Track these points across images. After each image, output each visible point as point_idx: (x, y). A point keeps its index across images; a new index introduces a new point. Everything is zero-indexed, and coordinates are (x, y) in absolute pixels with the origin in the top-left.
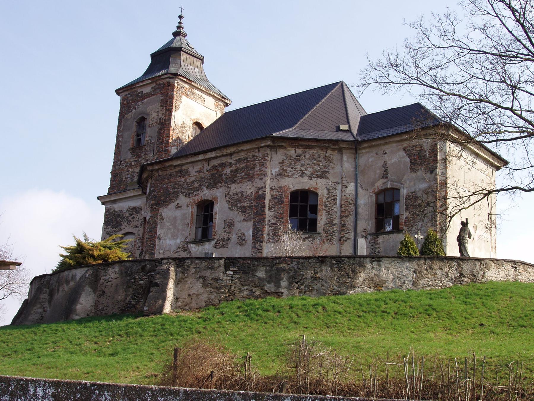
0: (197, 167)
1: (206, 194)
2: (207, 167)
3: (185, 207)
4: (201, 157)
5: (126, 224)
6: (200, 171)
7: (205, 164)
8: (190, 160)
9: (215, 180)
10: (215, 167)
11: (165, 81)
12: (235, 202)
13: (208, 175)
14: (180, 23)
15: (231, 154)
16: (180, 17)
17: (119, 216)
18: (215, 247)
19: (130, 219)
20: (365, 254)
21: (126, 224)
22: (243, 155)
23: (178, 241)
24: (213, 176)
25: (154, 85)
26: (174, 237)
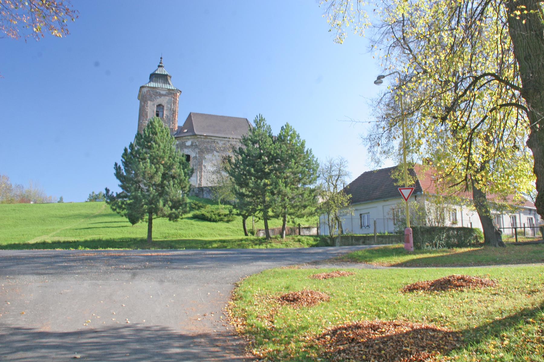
0: (223, 142)
6: (224, 144)
8: (221, 139)
16: (161, 58)
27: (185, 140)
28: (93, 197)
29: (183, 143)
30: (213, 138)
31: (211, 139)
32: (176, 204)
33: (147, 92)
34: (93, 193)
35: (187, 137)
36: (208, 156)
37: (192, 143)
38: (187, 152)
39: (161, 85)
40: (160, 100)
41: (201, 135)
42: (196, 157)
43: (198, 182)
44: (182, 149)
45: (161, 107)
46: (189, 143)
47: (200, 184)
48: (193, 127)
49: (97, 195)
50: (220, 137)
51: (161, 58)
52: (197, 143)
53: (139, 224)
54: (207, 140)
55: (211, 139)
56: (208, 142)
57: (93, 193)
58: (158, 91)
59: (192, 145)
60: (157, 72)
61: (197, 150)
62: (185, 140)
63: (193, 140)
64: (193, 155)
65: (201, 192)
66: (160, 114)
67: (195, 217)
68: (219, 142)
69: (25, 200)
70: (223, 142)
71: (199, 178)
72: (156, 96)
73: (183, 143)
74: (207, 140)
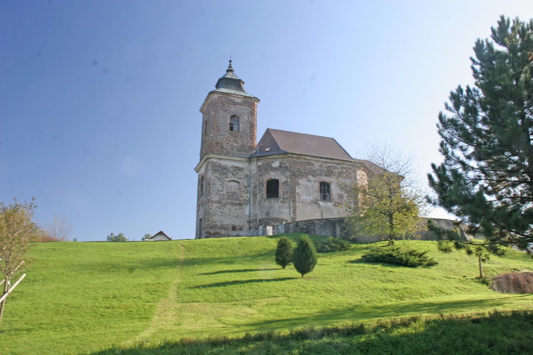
0: (319, 164)
1: (327, 179)
2: (325, 166)
3: (313, 182)
4: (323, 160)
5: (231, 175)
6: (320, 166)
7: (324, 164)
8: (317, 159)
9: (329, 173)
10: (329, 167)
11: (252, 101)
12: (343, 187)
13: (326, 170)
14: (230, 64)
15: (339, 164)
16: (230, 61)
17: (225, 168)
18: (334, 205)
19: (234, 172)
20: (291, 221)
21: (231, 175)
22: (344, 166)
23: (311, 198)
24: (328, 171)
25: (243, 100)
26: (308, 195)
27: (270, 160)
28: (111, 239)
29: (268, 164)
30: (307, 158)
31: (305, 159)
32: (215, 247)
33: (219, 98)
34: (112, 234)
35: (274, 156)
36: (302, 182)
37: (281, 164)
38: (273, 175)
39: (234, 91)
40: (233, 109)
41: (292, 154)
42: (287, 182)
43: (292, 215)
44: (266, 171)
45: (236, 118)
46: (276, 164)
47: (293, 219)
48: (277, 145)
49: (116, 237)
50: (316, 157)
51: (230, 61)
52: (288, 164)
53: (287, 267)
54: (300, 161)
55: (305, 159)
56: (301, 163)
57: (112, 234)
58: (231, 98)
59: (280, 167)
60: (227, 76)
61: (288, 174)
62: (270, 160)
63: (282, 160)
64: (282, 179)
65: (312, 227)
66: (235, 127)
67: (372, 259)
68: (314, 163)
69: (48, 240)
70: (319, 164)
71: (292, 210)
72: (229, 104)
73: (268, 164)
74: (300, 161)
